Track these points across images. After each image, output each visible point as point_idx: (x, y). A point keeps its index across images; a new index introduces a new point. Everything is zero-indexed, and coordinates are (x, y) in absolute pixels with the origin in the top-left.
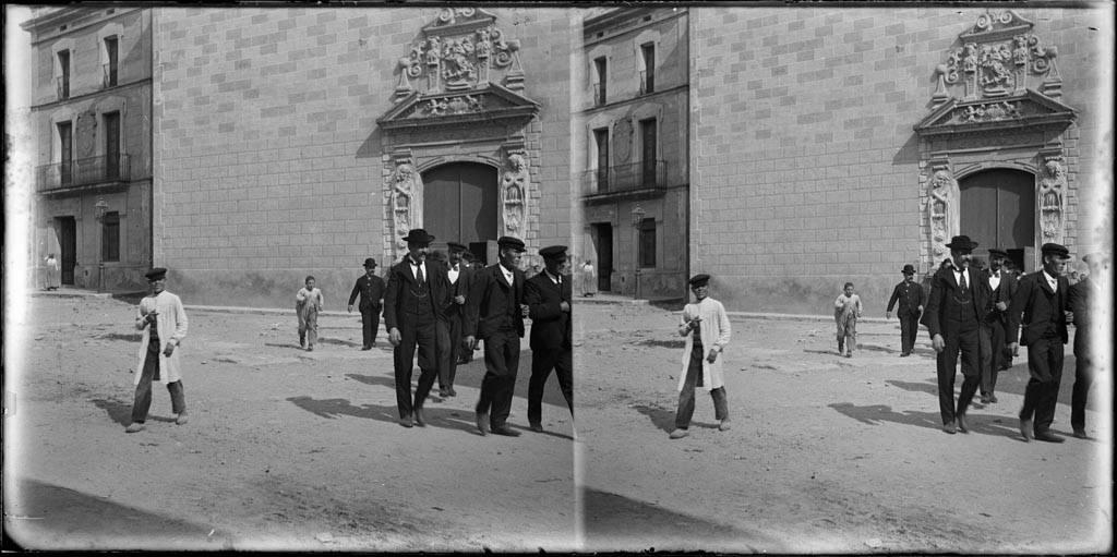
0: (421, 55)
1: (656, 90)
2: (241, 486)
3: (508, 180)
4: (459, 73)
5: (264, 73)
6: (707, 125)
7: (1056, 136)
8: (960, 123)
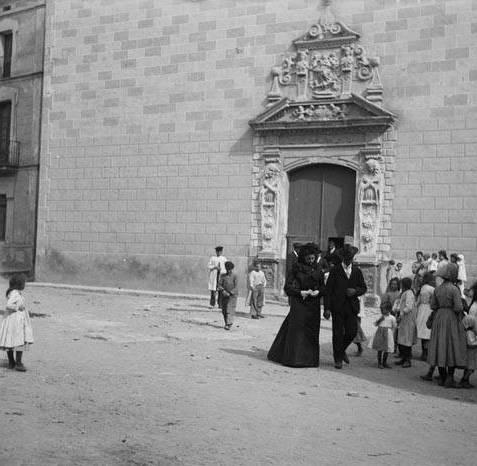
0: (292, 66)
1: (12, 75)
2: (98, 454)
3: (365, 182)
4: (325, 83)
5: (148, 72)
6: (59, 111)
7: (376, 137)
8: (291, 121)
